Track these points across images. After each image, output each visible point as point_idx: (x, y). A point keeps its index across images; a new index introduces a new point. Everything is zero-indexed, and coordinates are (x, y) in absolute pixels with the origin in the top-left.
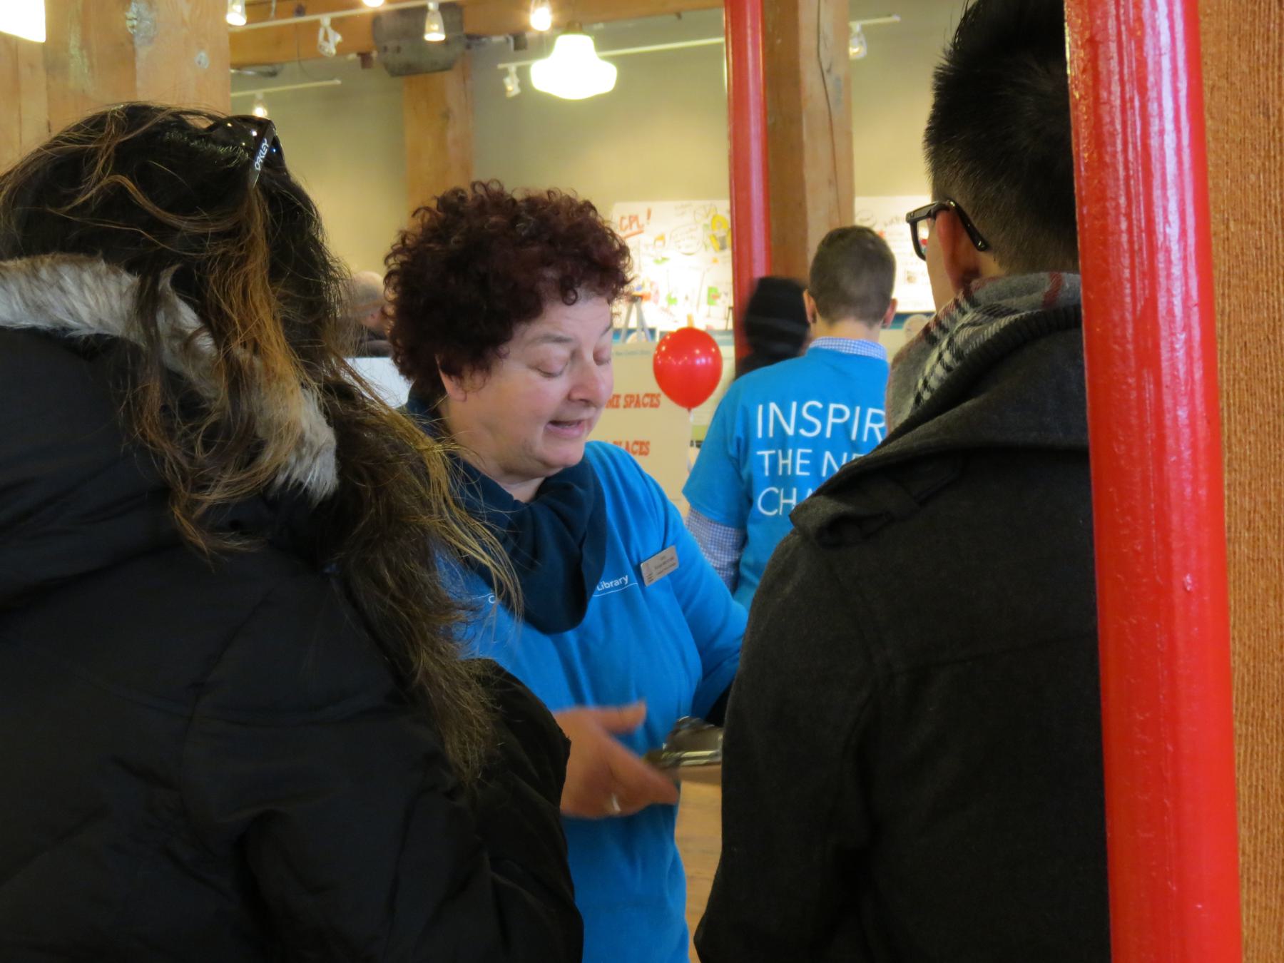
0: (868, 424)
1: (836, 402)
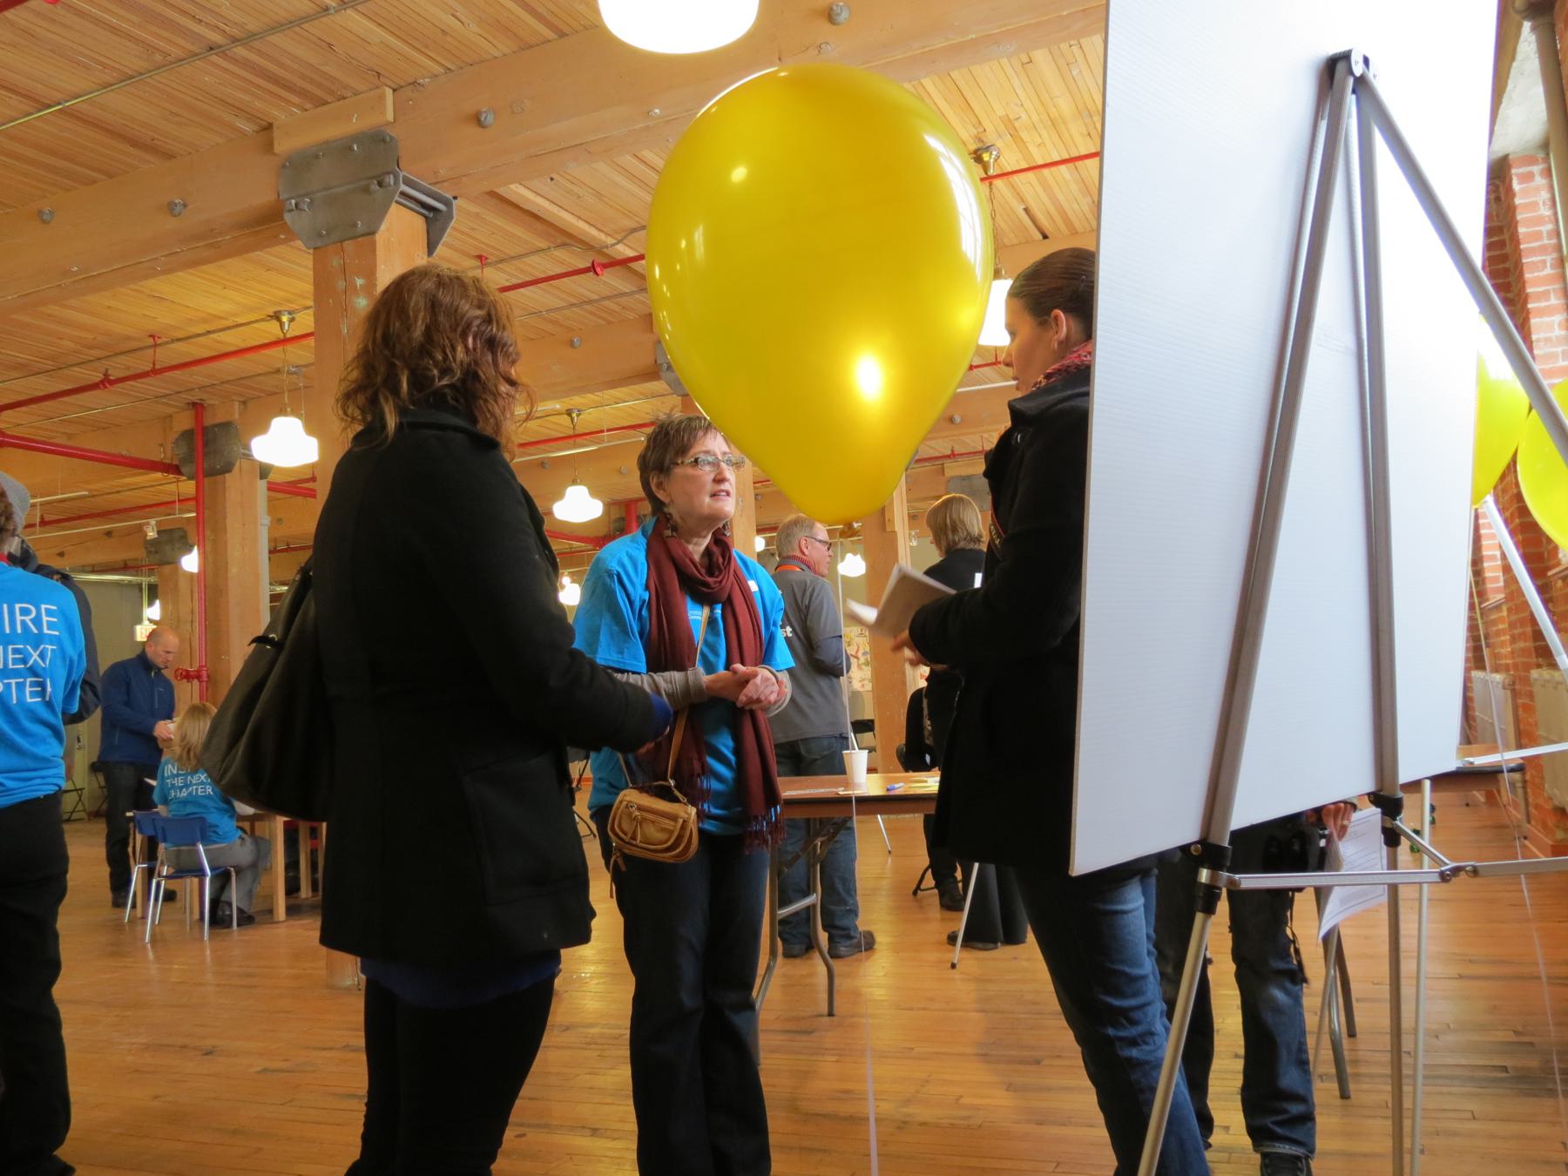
0: (19, 618)
1: (18, 603)
